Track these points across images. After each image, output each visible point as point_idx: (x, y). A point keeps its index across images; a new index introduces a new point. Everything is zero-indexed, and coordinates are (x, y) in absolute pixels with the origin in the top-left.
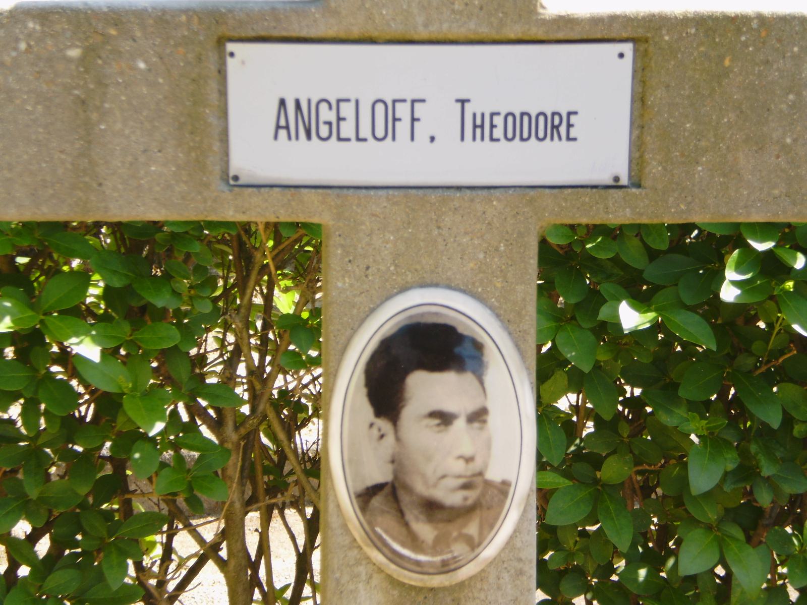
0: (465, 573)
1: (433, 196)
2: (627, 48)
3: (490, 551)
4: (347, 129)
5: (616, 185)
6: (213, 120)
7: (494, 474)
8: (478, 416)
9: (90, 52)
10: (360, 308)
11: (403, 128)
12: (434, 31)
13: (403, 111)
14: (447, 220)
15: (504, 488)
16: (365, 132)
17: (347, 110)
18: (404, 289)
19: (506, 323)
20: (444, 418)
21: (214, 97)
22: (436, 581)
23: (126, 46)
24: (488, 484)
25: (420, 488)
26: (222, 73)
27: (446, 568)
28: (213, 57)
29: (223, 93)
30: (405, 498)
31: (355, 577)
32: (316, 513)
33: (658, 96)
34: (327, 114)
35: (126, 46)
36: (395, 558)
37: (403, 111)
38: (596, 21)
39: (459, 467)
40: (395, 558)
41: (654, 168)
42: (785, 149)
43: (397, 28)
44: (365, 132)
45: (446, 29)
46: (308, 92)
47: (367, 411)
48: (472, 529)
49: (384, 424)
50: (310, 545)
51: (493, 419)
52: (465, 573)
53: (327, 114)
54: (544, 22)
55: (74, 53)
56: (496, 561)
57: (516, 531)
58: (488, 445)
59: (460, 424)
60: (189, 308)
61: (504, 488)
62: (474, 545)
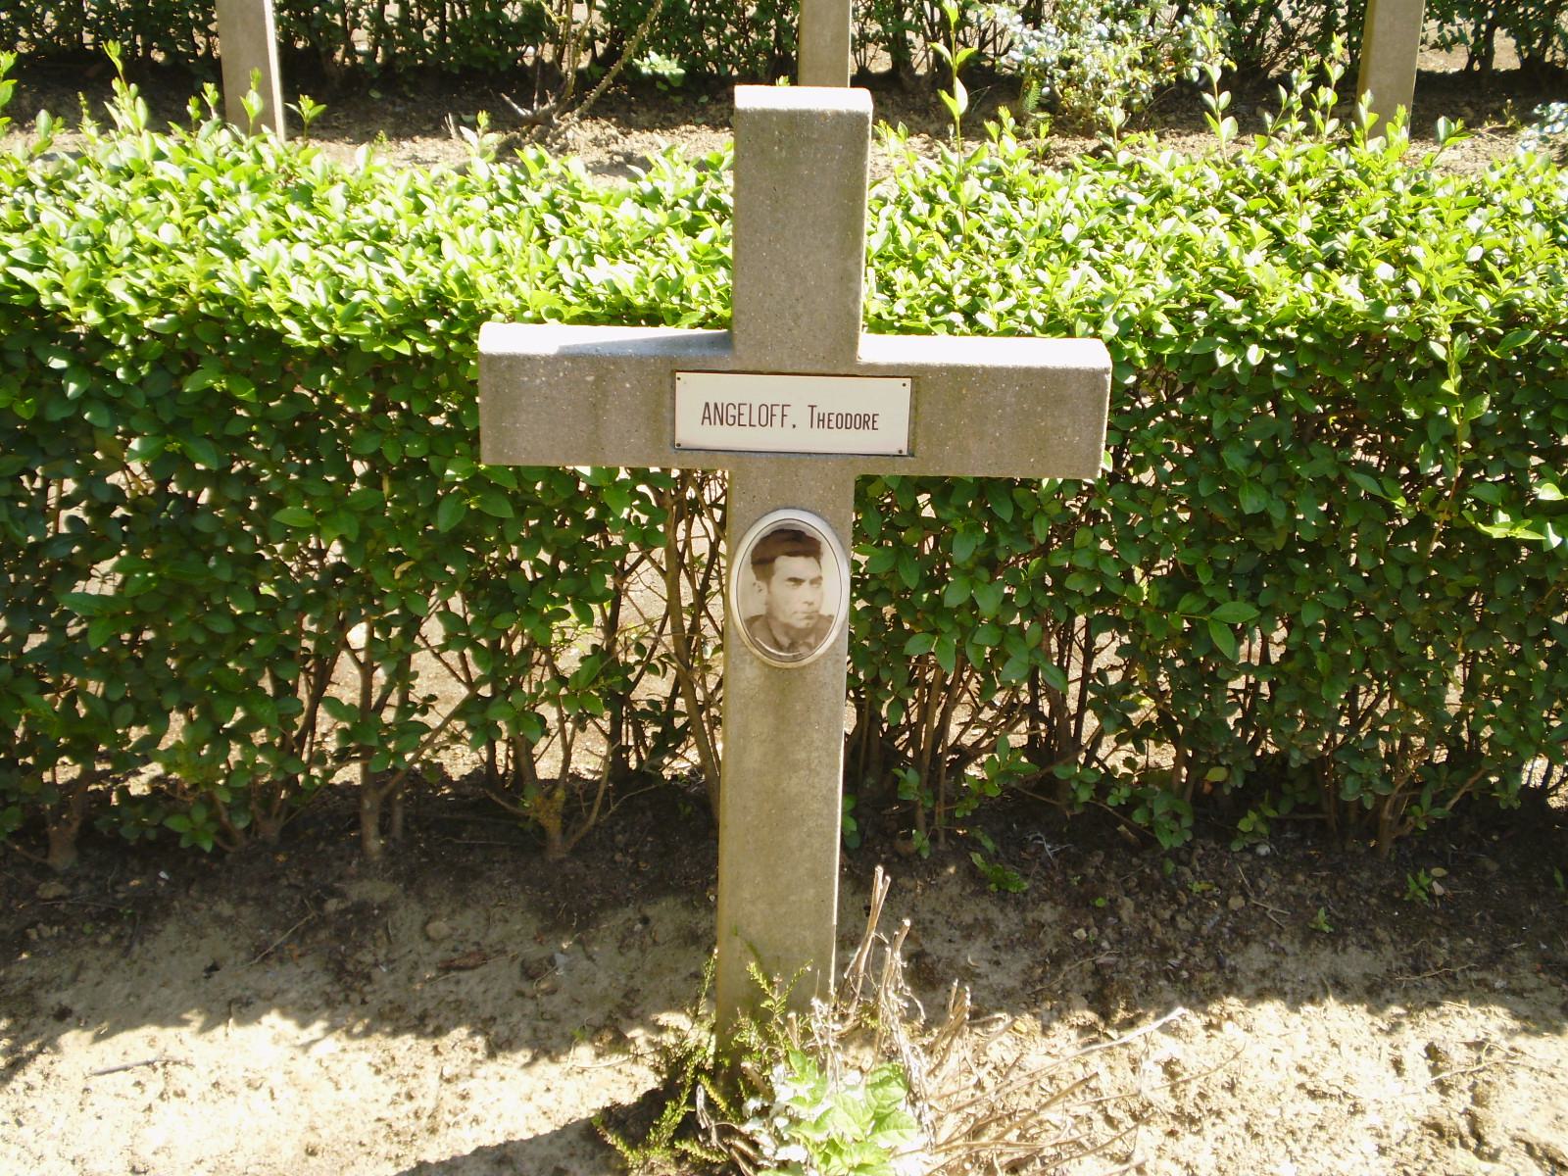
0: (805, 662)
1: (793, 458)
2: (908, 381)
3: (820, 651)
4: (744, 420)
5: (900, 455)
6: (667, 415)
7: (824, 612)
8: (816, 581)
9: (599, 379)
10: (931, 816)
11: (777, 420)
12: (796, 369)
13: (777, 411)
14: (802, 472)
15: (829, 619)
16: (755, 421)
17: (745, 410)
18: (776, 509)
19: (834, 529)
20: (797, 581)
21: (668, 402)
22: (790, 665)
23: (620, 375)
24: (821, 617)
25: (782, 618)
26: (673, 388)
27: (795, 659)
28: (668, 380)
29: (673, 398)
30: (773, 624)
31: (743, 661)
32: (724, 517)
33: (924, 408)
34: (732, 411)
35: (620, 375)
36: (767, 653)
37: (777, 411)
38: (889, 367)
39: (805, 607)
40: (767, 653)
41: (922, 448)
42: (996, 439)
43: (774, 368)
44: (755, 421)
45: (802, 369)
46: (722, 398)
47: (752, 576)
48: (811, 640)
49: (762, 584)
50: (718, 540)
51: (825, 583)
52: (805, 662)
53: (732, 411)
54: (860, 367)
55: (590, 379)
56: (823, 656)
57: (837, 640)
58: (822, 595)
59: (806, 585)
60: (270, 691)
61: (829, 619)
62: (812, 648)
